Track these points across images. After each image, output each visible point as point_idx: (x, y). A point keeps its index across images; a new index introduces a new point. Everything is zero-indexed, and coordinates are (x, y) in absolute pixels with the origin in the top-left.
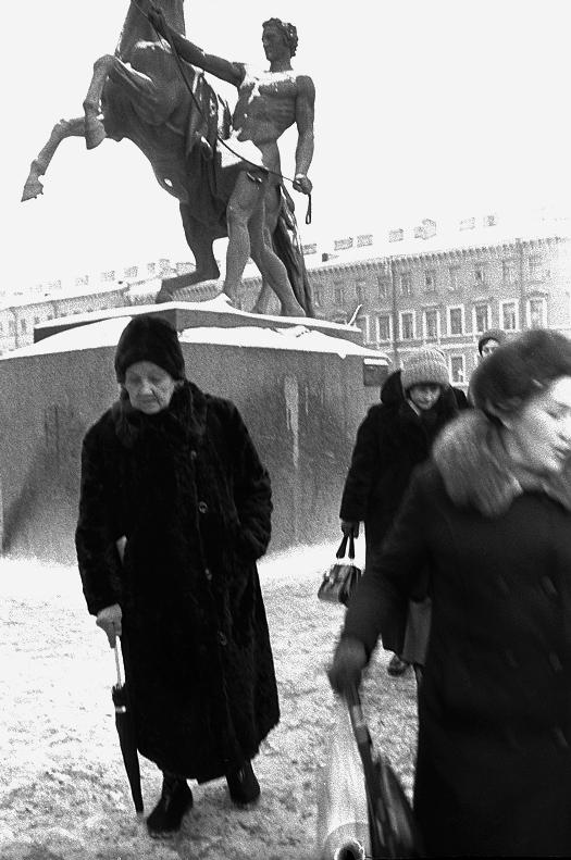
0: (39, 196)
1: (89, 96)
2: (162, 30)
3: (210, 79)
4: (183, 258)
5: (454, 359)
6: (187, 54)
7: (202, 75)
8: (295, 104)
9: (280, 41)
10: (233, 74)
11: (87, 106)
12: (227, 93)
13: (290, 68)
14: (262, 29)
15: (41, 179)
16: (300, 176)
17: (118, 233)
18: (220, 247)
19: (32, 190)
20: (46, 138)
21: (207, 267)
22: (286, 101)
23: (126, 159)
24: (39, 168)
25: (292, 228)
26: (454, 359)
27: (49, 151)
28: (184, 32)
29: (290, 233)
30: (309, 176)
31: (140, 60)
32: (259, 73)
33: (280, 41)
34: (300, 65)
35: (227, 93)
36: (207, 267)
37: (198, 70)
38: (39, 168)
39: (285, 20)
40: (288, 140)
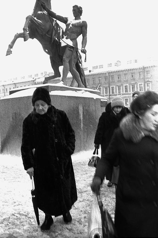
0: (11, 54)
1: (25, 27)
2: (45, 8)
3: (58, 22)
4: (51, 71)
5: (126, 99)
6: (52, 15)
7: (56, 21)
8: (82, 29)
9: (78, 11)
10: (65, 20)
11: (24, 29)
12: (63, 26)
13: (80, 19)
14: (73, 8)
15: (11, 49)
16: (83, 49)
17: (33, 64)
18: (61, 68)
19: (9, 53)
20: (13, 38)
21: (57, 74)
22: (79, 28)
23: (35, 44)
24: (11, 46)
25: (81, 63)
26: (126, 99)
27: (14, 42)
28: (51, 9)
29: (80, 64)
30: (86, 49)
31: (39, 17)
32: (72, 20)
33: (78, 11)
34: (83, 18)
35: (63, 26)
36: (57, 74)
37: (55, 19)
38: (11, 46)
39: (79, 6)
40: (80, 39)
